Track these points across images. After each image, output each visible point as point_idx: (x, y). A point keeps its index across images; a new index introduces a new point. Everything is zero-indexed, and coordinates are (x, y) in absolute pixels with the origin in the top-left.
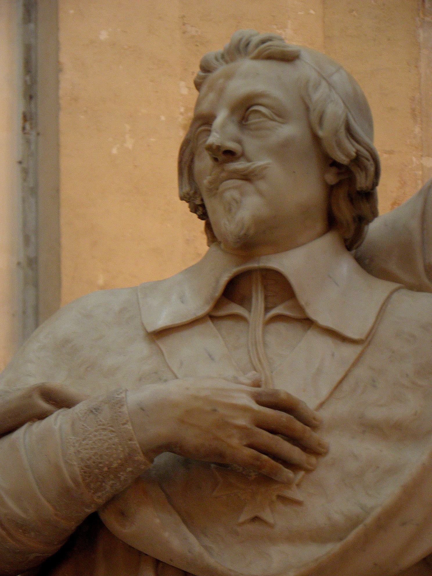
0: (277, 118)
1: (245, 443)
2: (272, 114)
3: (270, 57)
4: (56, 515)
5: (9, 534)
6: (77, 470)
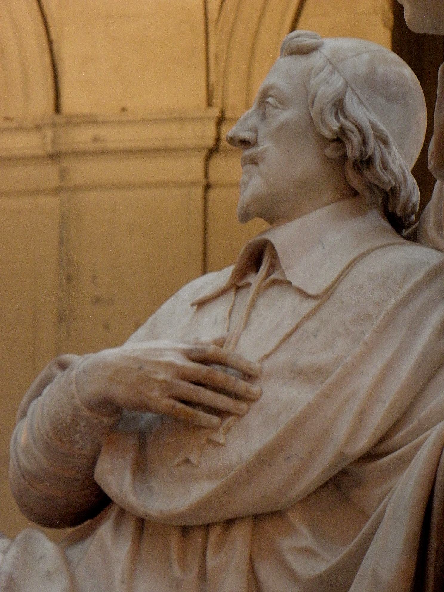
0: (279, 106)
1: (166, 395)
3: (292, 53)
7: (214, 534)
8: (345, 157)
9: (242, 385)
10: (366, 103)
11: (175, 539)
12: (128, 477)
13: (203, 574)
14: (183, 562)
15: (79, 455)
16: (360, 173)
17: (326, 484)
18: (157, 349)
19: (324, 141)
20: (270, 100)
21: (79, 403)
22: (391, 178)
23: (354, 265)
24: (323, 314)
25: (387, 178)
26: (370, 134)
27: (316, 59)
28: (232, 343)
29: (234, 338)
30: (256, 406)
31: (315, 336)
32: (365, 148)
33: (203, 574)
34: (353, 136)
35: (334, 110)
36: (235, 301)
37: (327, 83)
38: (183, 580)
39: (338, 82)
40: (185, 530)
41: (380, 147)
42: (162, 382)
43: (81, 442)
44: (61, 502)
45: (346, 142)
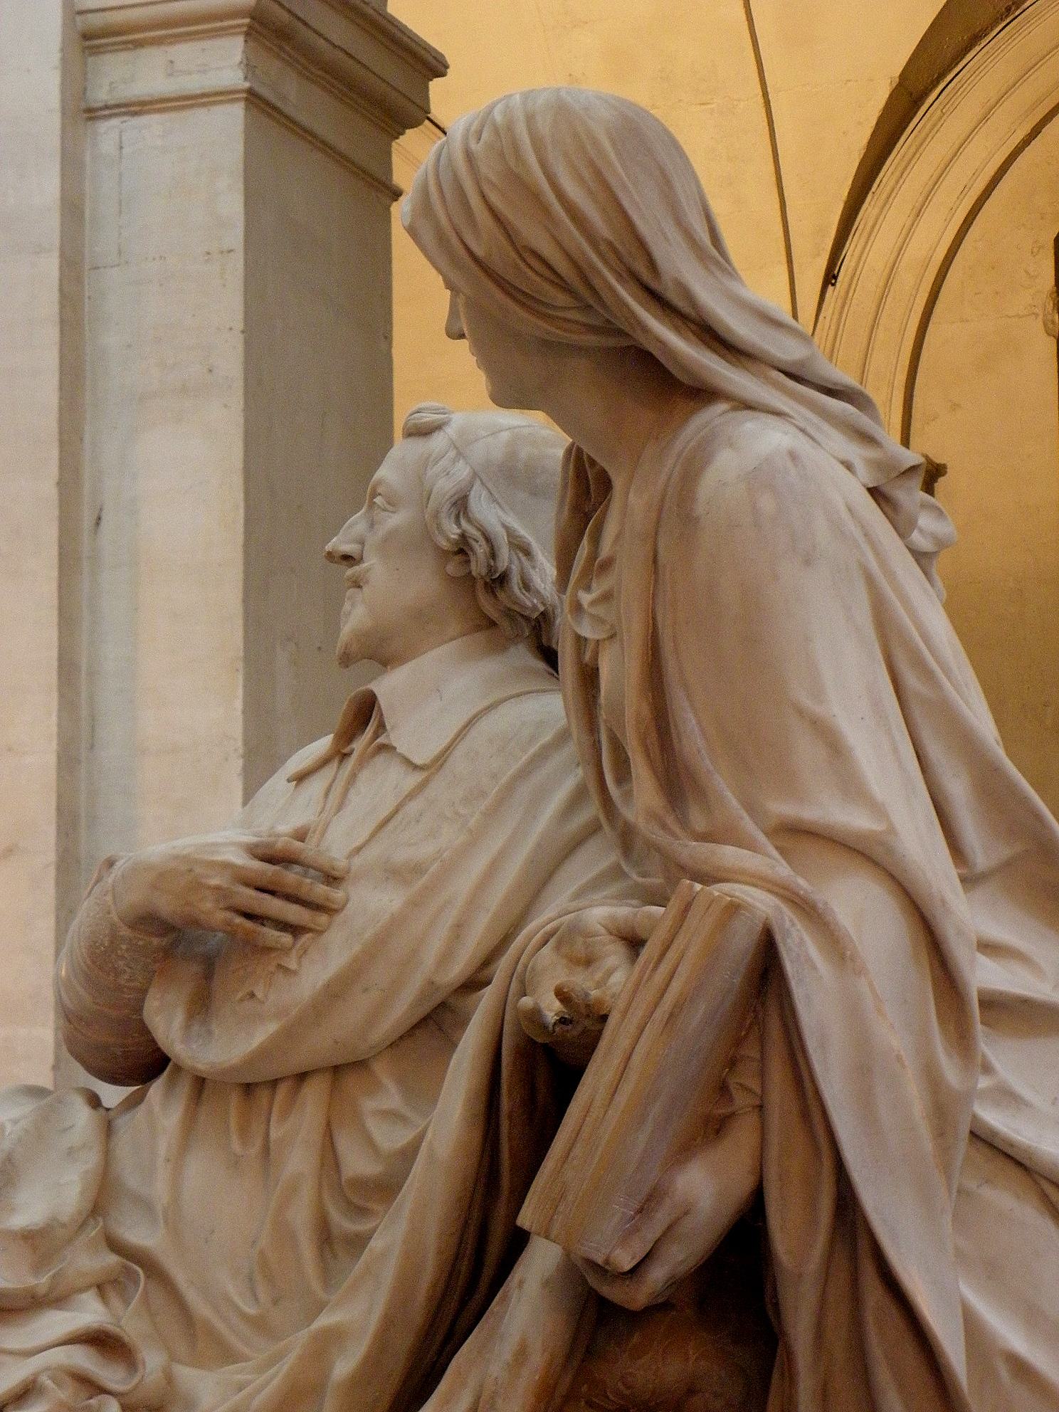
0: (388, 507)
7: (283, 1091)
9: (320, 891)
11: (235, 1099)
12: (179, 1017)
13: (266, 1150)
14: (244, 1132)
15: (128, 988)
18: (214, 844)
19: (444, 555)
20: (378, 500)
21: (116, 919)
22: (535, 601)
24: (431, 792)
25: (528, 600)
27: (438, 442)
28: (317, 836)
30: (339, 918)
32: (495, 562)
33: (266, 1150)
35: (455, 512)
39: (462, 471)
40: (248, 1089)
41: (519, 559)
42: (218, 888)
43: (128, 970)
44: (119, 1051)
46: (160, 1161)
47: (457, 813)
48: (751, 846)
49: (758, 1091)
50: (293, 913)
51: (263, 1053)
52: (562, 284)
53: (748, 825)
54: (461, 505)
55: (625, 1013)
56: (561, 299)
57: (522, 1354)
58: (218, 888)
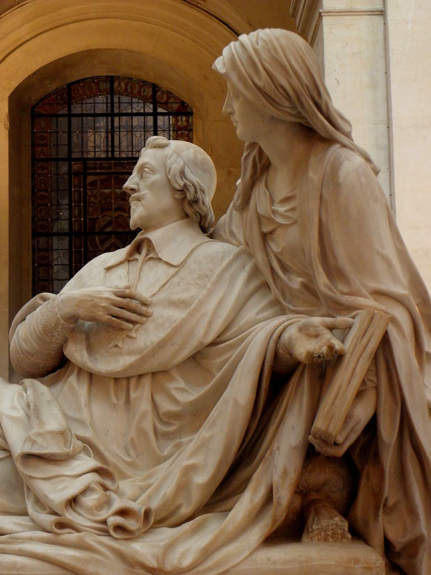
0: (152, 173)
2: (150, 171)
4: (40, 348)
5: (26, 357)
6: (40, 329)
7: (133, 382)
8: (185, 198)
9: (144, 309)
10: (194, 172)
12: (85, 354)
14: (116, 395)
16: (191, 205)
17: (188, 358)
21: (60, 317)
23: (194, 251)
26: (198, 188)
29: (135, 285)
31: (179, 285)
33: (128, 400)
34: (191, 189)
36: (129, 267)
37: (176, 162)
38: (117, 404)
43: (57, 336)
44: (41, 365)
45: (187, 191)
46: (83, 405)
47: (195, 283)
48: (365, 297)
49: (375, 381)
50: (134, 317)
51: (132, 366)
52: (288, 97)
53: (364, 291)
54: (182, 174)
55: (352, 354)
56: (287, 104)
57: (285, 473)
58: (105, 307)
